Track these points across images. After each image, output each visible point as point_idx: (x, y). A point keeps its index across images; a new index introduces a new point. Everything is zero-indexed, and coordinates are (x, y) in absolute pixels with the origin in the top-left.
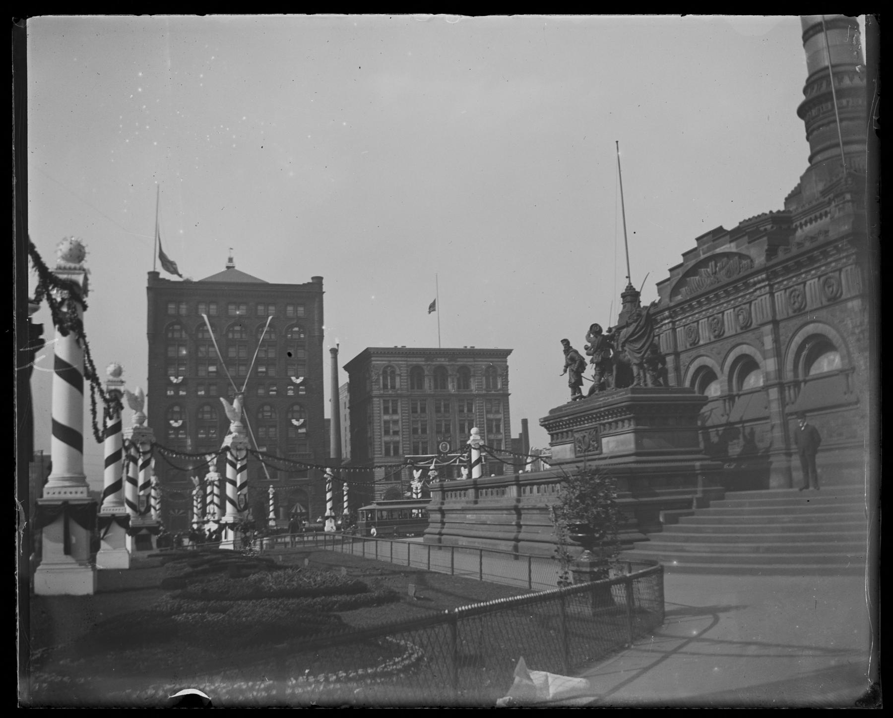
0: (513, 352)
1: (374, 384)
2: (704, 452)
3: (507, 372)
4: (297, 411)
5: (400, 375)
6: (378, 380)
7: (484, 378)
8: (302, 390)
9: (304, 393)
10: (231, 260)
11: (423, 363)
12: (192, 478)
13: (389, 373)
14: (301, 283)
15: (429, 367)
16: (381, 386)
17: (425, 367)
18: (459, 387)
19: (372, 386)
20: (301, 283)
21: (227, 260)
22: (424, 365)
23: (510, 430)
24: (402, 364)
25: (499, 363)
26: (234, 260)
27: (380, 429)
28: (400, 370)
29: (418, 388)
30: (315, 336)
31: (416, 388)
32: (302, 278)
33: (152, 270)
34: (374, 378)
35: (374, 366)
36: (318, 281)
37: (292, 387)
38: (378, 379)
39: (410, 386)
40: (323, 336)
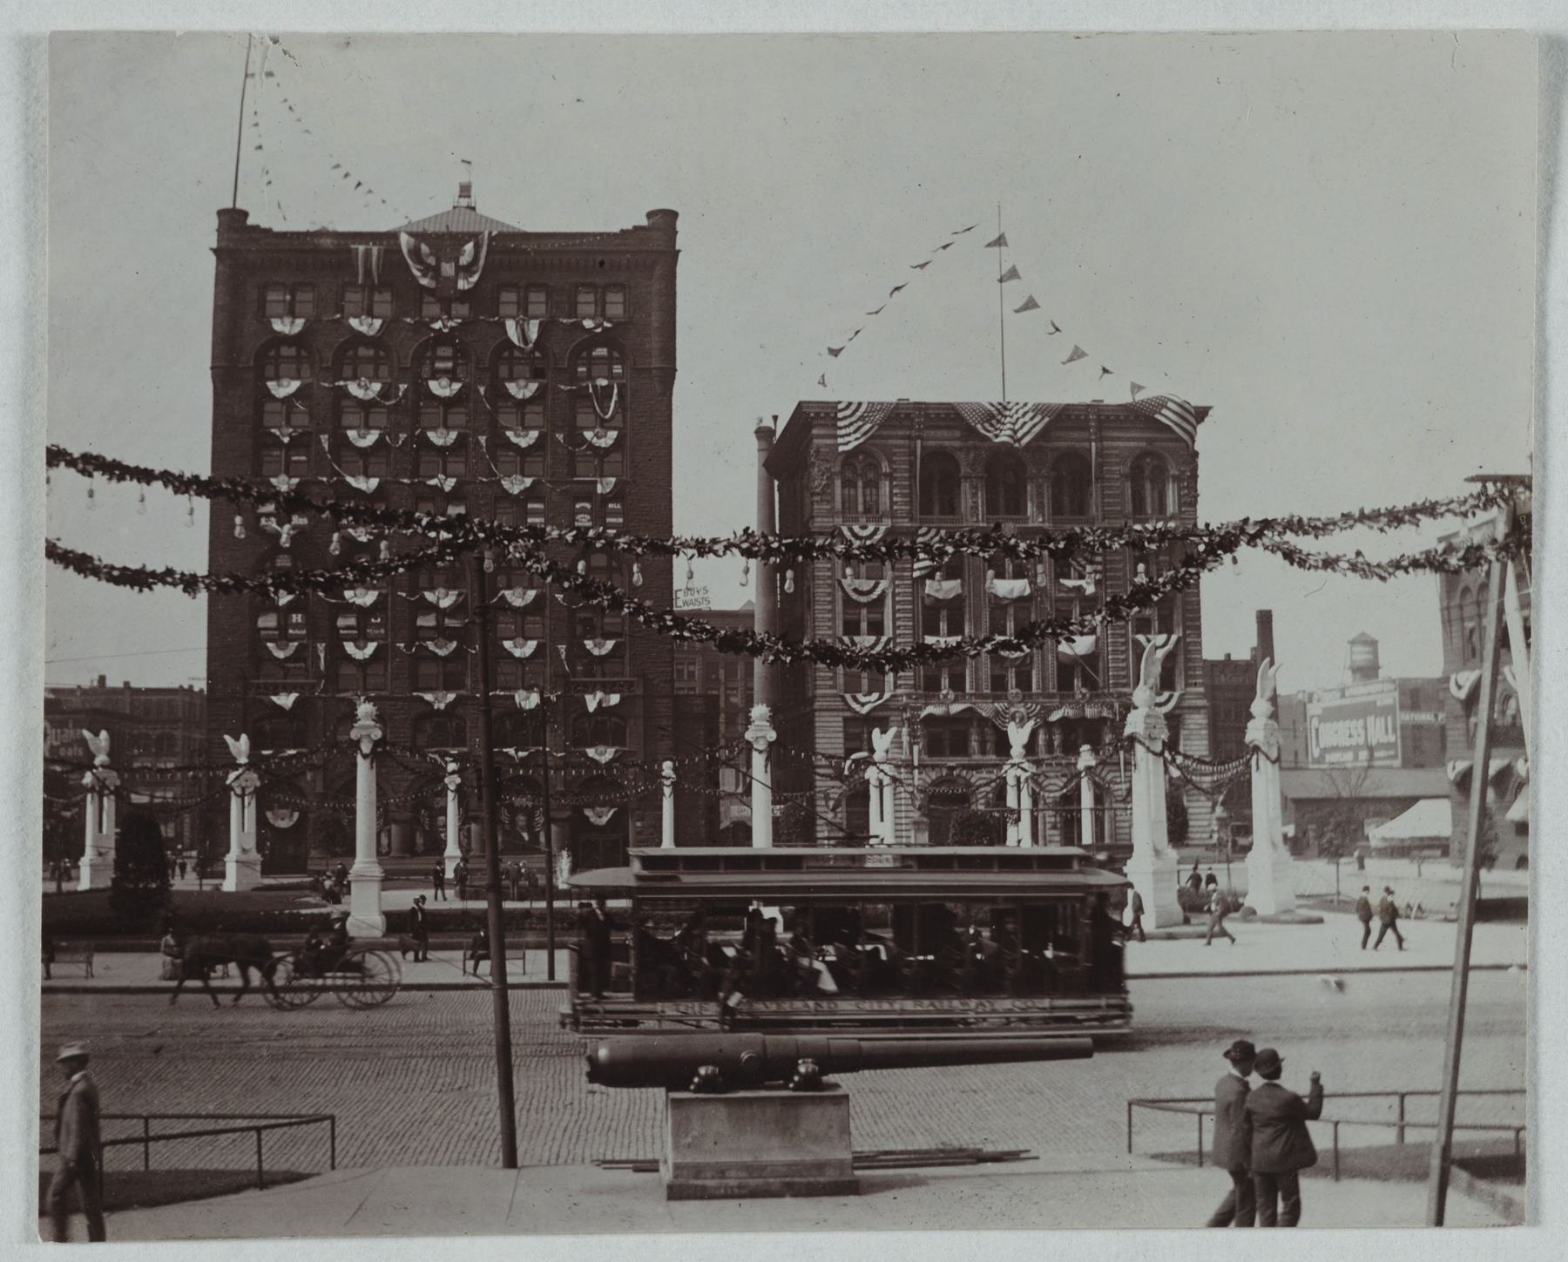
0: (1211, 413)
1: (817, 498)
2: (1008, 664)
3: (1195, 468)
4: (600, 568)
5: (890, 477)
6: (827, 491)
7: (1128, 484)
8: (615, 514)
9: (530, 506)
10: (465, 190)
11: (957, 444)
12: (228, 738)
13: (860, 465)
14: (679, 269)
15: (972, 456)
16: (838, 505)
17: (961, 456)
18: (1057, 510)
19: (812, 503)
20: (616, 229)
21: (457, 191)
22: (960, 449)
23: (1199, 628)
24: (896, 446)
25: (1170, 444)
26: (474, 192)
27: (833, 620)
28: (891, 462)
29: (942, 512)
30: (650, 370)
31: (937, 509)
32: (623, 215)
33: (229, 205)
34: (818, 483)
35: (818, 452)
36: (665, 221)
37: (588, 506)
38: (830, 485)
39: (917, 505)
40: (675, 370)
